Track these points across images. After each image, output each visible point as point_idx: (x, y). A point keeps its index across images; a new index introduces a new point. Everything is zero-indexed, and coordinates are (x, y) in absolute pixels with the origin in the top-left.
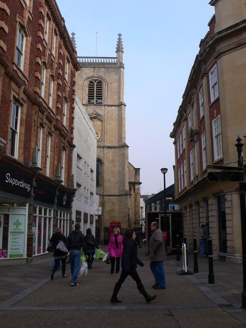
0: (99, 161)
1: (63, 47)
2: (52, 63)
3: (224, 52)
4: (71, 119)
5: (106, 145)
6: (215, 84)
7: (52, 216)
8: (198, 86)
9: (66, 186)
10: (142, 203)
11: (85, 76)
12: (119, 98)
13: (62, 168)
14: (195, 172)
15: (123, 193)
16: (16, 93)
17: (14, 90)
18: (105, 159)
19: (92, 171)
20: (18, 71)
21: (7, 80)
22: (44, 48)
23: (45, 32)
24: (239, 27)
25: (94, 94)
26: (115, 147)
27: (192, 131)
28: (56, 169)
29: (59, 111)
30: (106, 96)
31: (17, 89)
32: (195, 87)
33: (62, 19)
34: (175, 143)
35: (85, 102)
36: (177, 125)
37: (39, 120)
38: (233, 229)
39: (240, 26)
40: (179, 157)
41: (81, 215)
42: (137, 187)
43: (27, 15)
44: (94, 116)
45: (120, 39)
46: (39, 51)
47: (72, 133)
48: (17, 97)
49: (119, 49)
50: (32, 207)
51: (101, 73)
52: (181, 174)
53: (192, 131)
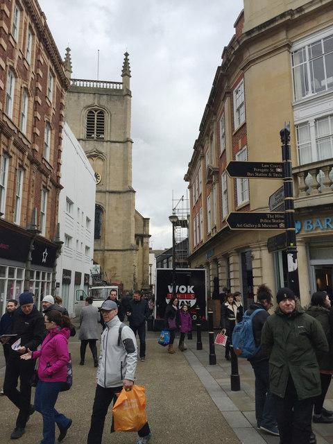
0: (99, 210)
1: (43, 52)
3: (253, 61)
4: (58, 153)
6: (241, 106)
7: (23, 278)
8: (219, 111)
9: (48, 238)
10: (152, 259)
11: (83, 104)
12: (125, 133)
13: (43, 214)
14: (213, 222)
15: (128, 247)
18: (107, 207)
19: (88, 220)
22: (12, 48)
23: (12, 24)
24: (272, 26)
27: (210, 170)
32: (215, 114)
33: (42, 14)
34: (190, 187)
35: (83, 136)
36: (193, 165)
40: (194, 204)
41: (70, 275)
42: (145, 240)
44: (94, 153)
45: (126, 60)
47: (58, 170)
49: (126, 72)
50: (29, 273)
51: (104, 101)
52: (196, 225)
53: (210, 170)
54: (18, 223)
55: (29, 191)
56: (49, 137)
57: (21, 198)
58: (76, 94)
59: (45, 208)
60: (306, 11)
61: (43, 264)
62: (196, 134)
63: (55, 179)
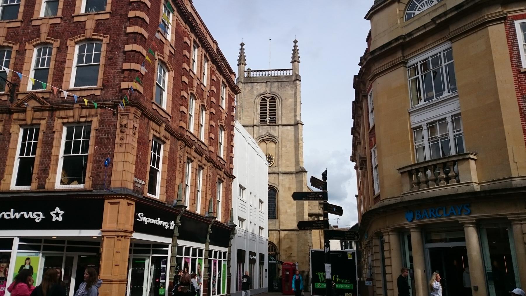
0: (273, 192)
2: (203, 93)
4: (230, 148)
5: (281, 170)
9: (223, 222)
11: (256, 93)
12: (295, 116)
16: (156, 132)
17: (153, 130)
18: (281, 187)
19: (261, 202)
20: (158, 110)
21: (146, 120)
22: (191, 78)
24: (390, 47)
25: (266, 113)
26: (291, 173)
28: (211, 203)
29: (214, 141)
30: (280, 115)
31: (157, 128)
37: (186, 155)
38: (392, 276)
39: (394, 45)
43: (167, 50)
44: (267, 137)
46: (184, 84)
48: (158, 135)
49: (295, 59)
51: (275, 88)
54: (198, 212)
55: (207, 184)
56: (223, 137)
57: (201, 191)
58: (250, 84)
59: (220, 196)
60: (415, 36)
62: (351, 123)
63: (228, 171)
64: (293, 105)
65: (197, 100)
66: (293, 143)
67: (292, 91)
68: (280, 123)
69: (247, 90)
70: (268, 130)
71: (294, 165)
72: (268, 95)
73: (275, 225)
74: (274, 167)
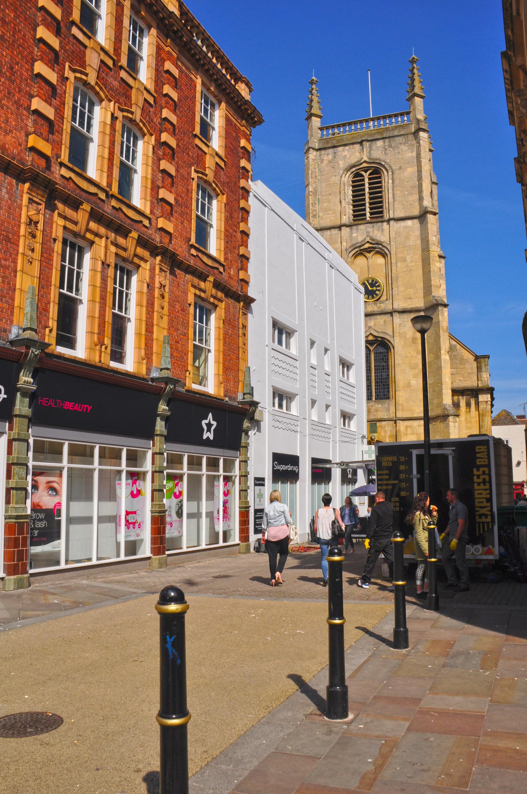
5: (396, 306)
11: (342, 164)
30: (391, 200)
44: (367, 245)
58: (331, 151)
61: (207, 443)
64: (416, 179)
65: (219, 197)
66: (419, 252)
67: (412, 152)
68: (391, 216)
69: (326, 162)
70: (368, 232)
71: (422, 295)
72: (365, 165)
73: (388, 410)
74: (383, 302)
